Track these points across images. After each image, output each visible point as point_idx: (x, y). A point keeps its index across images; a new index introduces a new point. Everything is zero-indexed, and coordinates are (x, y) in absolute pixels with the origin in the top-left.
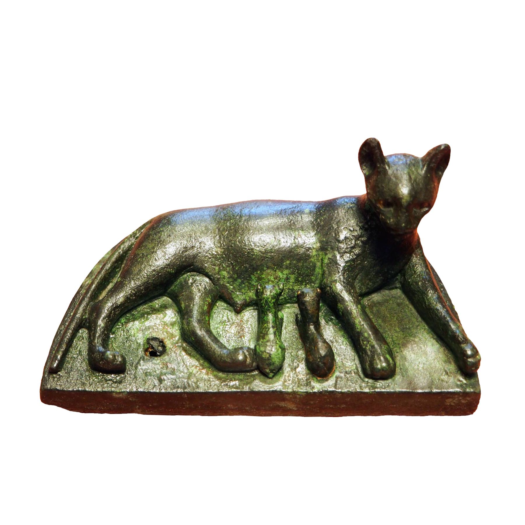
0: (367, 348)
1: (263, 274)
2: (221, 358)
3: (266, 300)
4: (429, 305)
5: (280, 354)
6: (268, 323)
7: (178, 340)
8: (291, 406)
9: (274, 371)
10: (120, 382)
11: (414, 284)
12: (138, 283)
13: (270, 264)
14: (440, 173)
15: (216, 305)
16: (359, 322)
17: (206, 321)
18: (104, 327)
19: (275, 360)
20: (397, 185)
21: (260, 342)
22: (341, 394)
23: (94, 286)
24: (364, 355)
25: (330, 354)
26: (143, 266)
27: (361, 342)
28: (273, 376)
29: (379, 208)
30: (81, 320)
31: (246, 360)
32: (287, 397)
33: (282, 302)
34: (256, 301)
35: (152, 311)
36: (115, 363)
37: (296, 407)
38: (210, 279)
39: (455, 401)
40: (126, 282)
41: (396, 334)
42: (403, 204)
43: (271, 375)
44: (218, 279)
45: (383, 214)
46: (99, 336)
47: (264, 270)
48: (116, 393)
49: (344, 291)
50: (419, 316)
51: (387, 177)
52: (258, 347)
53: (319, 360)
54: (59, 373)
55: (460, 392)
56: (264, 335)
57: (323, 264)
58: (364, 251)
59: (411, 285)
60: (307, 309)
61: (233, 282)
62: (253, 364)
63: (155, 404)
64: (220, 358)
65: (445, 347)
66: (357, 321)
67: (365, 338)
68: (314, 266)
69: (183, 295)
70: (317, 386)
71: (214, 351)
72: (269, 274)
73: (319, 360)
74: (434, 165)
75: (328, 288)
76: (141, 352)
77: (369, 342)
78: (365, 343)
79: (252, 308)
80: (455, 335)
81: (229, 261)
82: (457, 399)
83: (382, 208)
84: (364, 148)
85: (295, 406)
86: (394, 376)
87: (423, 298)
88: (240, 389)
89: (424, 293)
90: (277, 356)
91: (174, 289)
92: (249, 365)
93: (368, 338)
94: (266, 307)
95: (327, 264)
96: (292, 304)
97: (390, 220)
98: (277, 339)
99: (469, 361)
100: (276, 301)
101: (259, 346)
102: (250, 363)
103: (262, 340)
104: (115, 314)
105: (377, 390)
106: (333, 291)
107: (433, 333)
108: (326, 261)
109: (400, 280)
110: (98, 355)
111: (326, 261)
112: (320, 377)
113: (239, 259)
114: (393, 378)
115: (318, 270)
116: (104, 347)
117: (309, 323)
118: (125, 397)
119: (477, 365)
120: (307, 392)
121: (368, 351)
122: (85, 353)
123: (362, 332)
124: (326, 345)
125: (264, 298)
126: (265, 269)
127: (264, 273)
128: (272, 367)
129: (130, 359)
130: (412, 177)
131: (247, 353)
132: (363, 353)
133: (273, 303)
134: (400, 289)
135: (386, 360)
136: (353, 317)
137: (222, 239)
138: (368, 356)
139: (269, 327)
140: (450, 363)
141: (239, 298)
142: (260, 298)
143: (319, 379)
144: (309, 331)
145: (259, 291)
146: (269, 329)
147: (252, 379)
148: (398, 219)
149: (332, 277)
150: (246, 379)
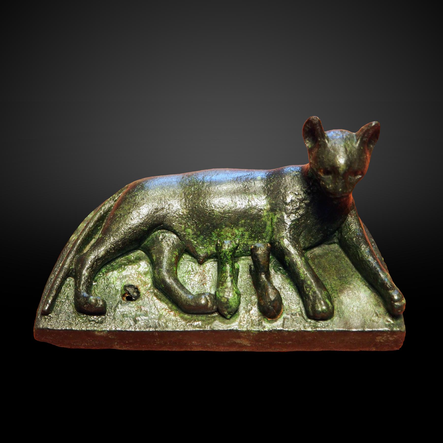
0: (310, 294)
1: (222, 231)
2: (187, 302)
3: (224, 253)
4: (362, 258)
5: (236, 299)
6: (226, 273)
7: (150, 287)
9: (231, 313)
10: (101, 322)
11: (350, 240)
12: (117, 239)
13: (228, 223)
15: (183, 258)
16: (303, 272)
17: (174, 271)
18: (88, 276)
19: (232, 304)
20: (335, 156)
21: (220, 289)
22: (288, 333)
23: (79, 241)
25: (279, 299)
26: (121, 224)
27: (305, 288)
28: (231, 317)
29: (320, 176)
30: (69, 270)
31: (208, 304)
32: (242, 335)
33: (238, 255)
34: (216, 254)
35: (128, 263)
36: (97, 306)
37: (250, 343)
38: (177, 235)
39: (384, 338)
40: (107, 238)
41: (334, 282)
42: (340, 172)
43: (229, 316)
44: (184, 236)
46: (84, 284)
47: (223, 228)
48: (98, 331)
49: (290, 246)
50: (353, 267)
51: (326, 149)
52: (217, 293)
53: (269, 304)
54: (50, 315)
55: (388, 330)
56: (223, 282)
57: (273, 223)
58: (307, 212)
59: (347, 240)
60: (259, 261)
61: (196, 238)
62: (213, 307)
63: (131, 341)
64: (186, 302)
65: (376, 293)
66: (301, 271)
67: (308, 285)
68: (265, 225)
69: (154, 249)
70: (268, 326)
71: (180, 296)
72: (227, 232)
73: (269, 304)
74: (366, 140)
75: (277, 243)
76: (119, 297)
77: (311, 288)
78: (308, 289)
79: (213, 260)
80: (384, 283)
82: (385, 337)
83: (322, 175)
84: (307, 125)
85: (249, 342)
86: (332, 317)
87: (357, 252)
88: (202, 328)
89: (358, 248)
90: (234, 301)
91: (147, 244)
92: (210, 308)
93: (311, 285)
94: (225, 259)
95: (276, 223)
96: (247, 257)
97: (329, 186)
98: (234, 286)
99: (396, 305)
100: (233, 254)
101: (219, 292)
102: (211, 306)
103: (221, 287)
104: (97, 265)
105: (318, 329)
106: (281, 246)
107: (365, 281)
108: (275, 220)
109: (337, 236)
110: (83, 300)
111: (275, 220)
112: (270, 318)
113: (202, 219)
114: (332, 319)
115: (268, 228)
116: (87, 293)
117: (261, 272)
118: (106, 335)
120: (259, 331)
121: (310, 296)
122: (72, 298)
123: (305, 280)
124: (275, 291)
125: (223, 252)
126: (224, 227)
127: (223, 230)
128: (229, 310)
129: (109, 303)
131: (208, 298)
132: (306, 298)
133: (231, 255)
134: (338, 244)
136: (298, 268)
138: (311, 300)
139: (227, 276)
140: (380, 306)
141: (202, 251)
142: (219, 251)
143: (269, 320)
144: (260, 279)
145: (218, 245)
146: (227, 277)
147: (213, 320)
148: (336, 185)
149: (280, 234)
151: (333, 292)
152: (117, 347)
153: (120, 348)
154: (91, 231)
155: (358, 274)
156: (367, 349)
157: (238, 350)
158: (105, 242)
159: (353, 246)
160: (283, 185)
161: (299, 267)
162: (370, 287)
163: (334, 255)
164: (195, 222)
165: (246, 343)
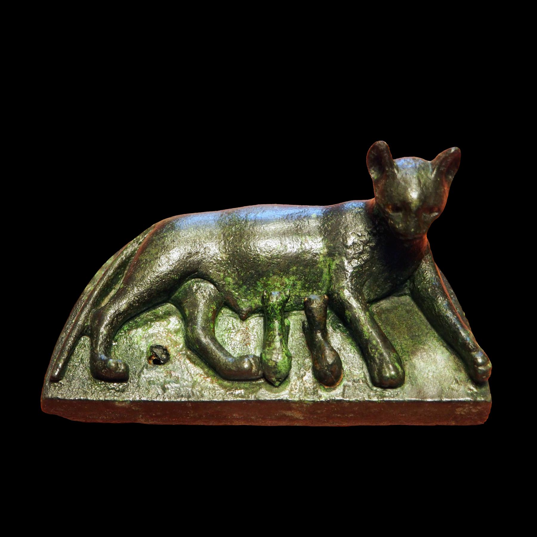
0: (376, 356)
1: (269, 280)
2: (226, 366)
3: (272, 307)
4: (439, 312)
5: (287, 362)
6: (274, 331)
7: (182, 348)
9: (280, 380)
10: (123, 391)
11: (424, 290)
12: (141, 289)
13: (276, 270)
15: (221, 312)
16: (367, 329)
17: (211, 328)
18: (106, 334)
19: (281, 368)
21: (266, 350)
22: (349, 403)
23: (96, 292)
24: (372, 363)
25: (338, 362)
26: (146, 272)
27: (369, 350)
28: (280, 385)
29: (388, 213)
30: (83, 327)
31: (252, 368)
32: (294, 406)
33: (288, 309)
34: (262, 307)
35: (156, 318)
36: (117, 371)
37: (303, 416)
38: (215, 285)
39: (465, 410)
41: (405, 342)
42: (412, 208)
43: (277, 384)
44: (223, 286)
45: (392, 219)
46: (102, 344)
47: (270, 277)
48: (119, 402)
49: (352, 298)
50: (428, 323)
51: (396, 181)
52: (263, 355)
53: (326, 368)
54: (60, 381)
55: (471, 400)
56: (270, 342)
57: (331, 270)
58: (372, 257)
59: (421, 291)
60: (314, 316)
61: (238, 288)
62: (259, 372)
63: (159, 413)
64: (225, 366)
65: (456, 355)
66: (365, 329)
67: (374, 345)
68: (322, 272)
69: (187, 302)
70: (325, 395)
71: (219, 359)
73: (326, 368)
74: (444, 169)
75: (336, 295)
76: (144, 360)
77: (377, 349)
78: (373, 350)
79: (258, 315)
80: (466, 343)
81: (235, 267)
83: (390, 212)
84: (372, 152)
85: (302, 415)
86: (403, 385)
87: (433, 305)
88: (245, 398)
89: (434, 300)
90: (284, 364)
91: (178, 296)
92: (254, 373)
93: (377, 346)
94: (272, 314)
95: (335, 270)
97: (399, 225)
98: (284, 346)
99: (480, 370)
100: (282, 308)
101: (265, 354)
102: (256, 371)
103: (268, 348)
104: (117, 321)
105: (385, 399)
106: (340, 298)
107: (443, 341)
108: (334, 267)
109: (409, 286)
110: (101, 364)
111: (333, 267)
112: (327, 385)
113: (245, 265)
114: (402, 387)
117: (316, 330)
118: (128, 406)
120: (314, 401)
121: (376, 359)
122: (87, 361)
123: (370, 340)
125: (270, 305)
126: (271, 275)
128: (278, 376)
129: (133, 367)
130: (421, 181)
131: (252, 361)
132: (371, 361)
133: (280, 309)
134: (409, 296)
135: (395, 368)
136: (361, 325)
138: (376, 364)
139: (275, 334)
140: (460, 371)
141: (245, 305)
142: (266, 305)
143: (326, 387)
144: (316, 338)
145: (265, 297)
146: (275, 336)
147: (258, 388)
149: (340, 283)
150: (251, 388)
151: (403, 354)
152: (142, 421)
153: (145, 421)
154: (111, 280)
155: (434, 332)
156: (445, 424)
157: (288, 424)
158: (127, 293)
161: (362, 324)
164: (237, 269)
165: (298, 415)
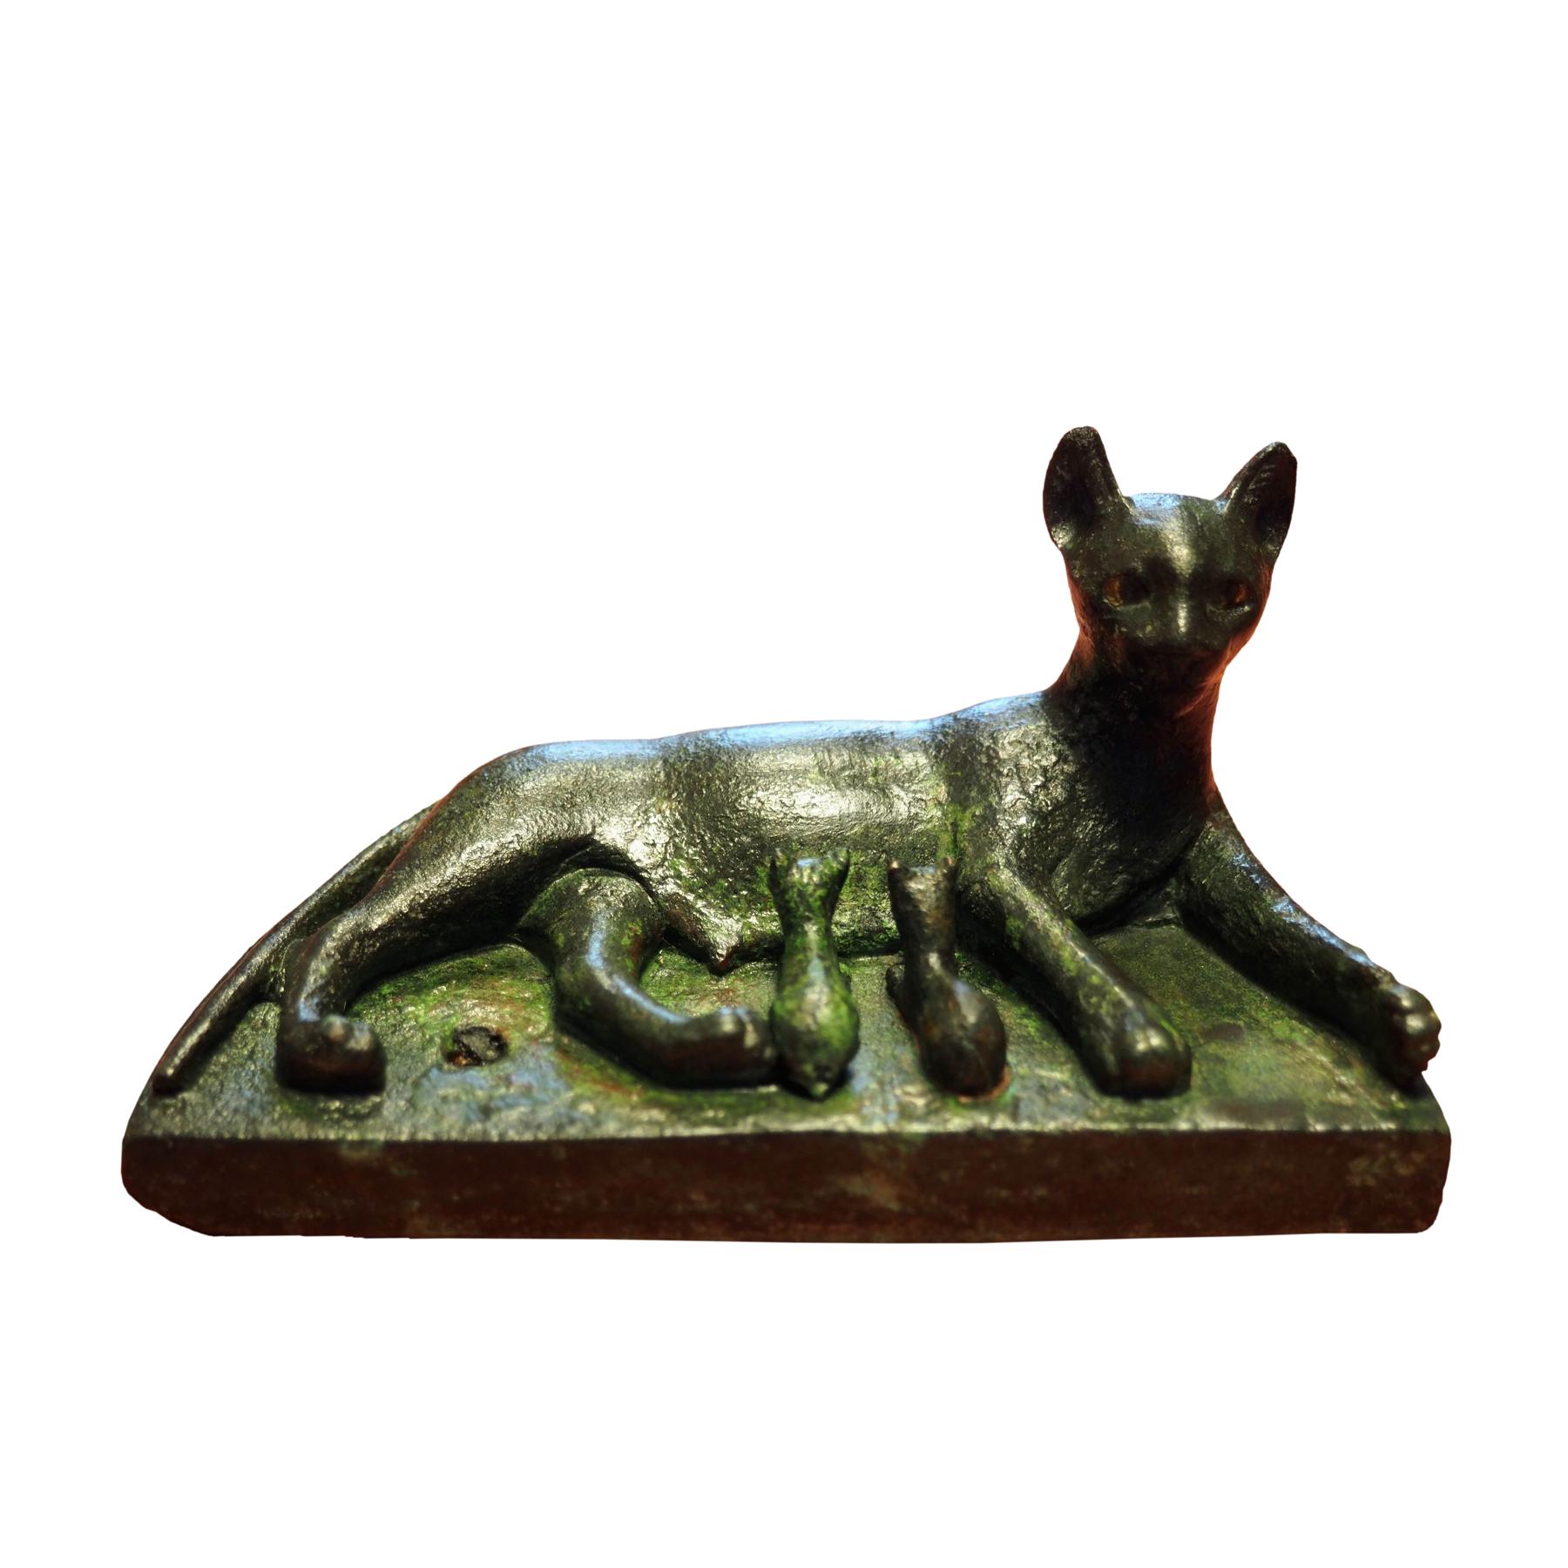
0: (1103, 1011)
4: (1268, 923)
8: (883, 1194)
14: (1271, 547)
16: (1071, 955)
18: (326, 976)
28: (829, 1094)
29: (1109, 610)
32: (870, 1151)
33: (845, 946)
37: (900, 1198)
41: (1180, 1013)
43: (822, 1088)
50: (1239, 976)
57: (958, 835)
58: (1072, 796)
59: (1211, 889)
60: (920, 912)
61: (703, 887)
65: (1329, 1031)
66: (1066, 954)
70: (957, 1121)
75: (977, 887)
76: (433, 1054)
78: (1094, 1000)
82: (1382, 1159)
83: (1119, 606)
91: (539, 911)
95: (970, 831)
96: (875, 958)
105: (1140, 1126)
106: (990, 891)
107: (1287, 1006)
108: (967, 824)
109: (1175, 897)
111: (966, 825)
113: (722, 824)
119: (1429, 1041)
128: (822, 1057)
133: (821, 898)
134: (1178, 925)
136: (1053, 945)
137: (675, 778)
138: (1106, 1029)
149: (985, 858)
155: (1258, 992)
158: (395, 887)
159: (1234, 899)
160: (985, 728)
162: (1305, 1020)
163: (1168, 953)
